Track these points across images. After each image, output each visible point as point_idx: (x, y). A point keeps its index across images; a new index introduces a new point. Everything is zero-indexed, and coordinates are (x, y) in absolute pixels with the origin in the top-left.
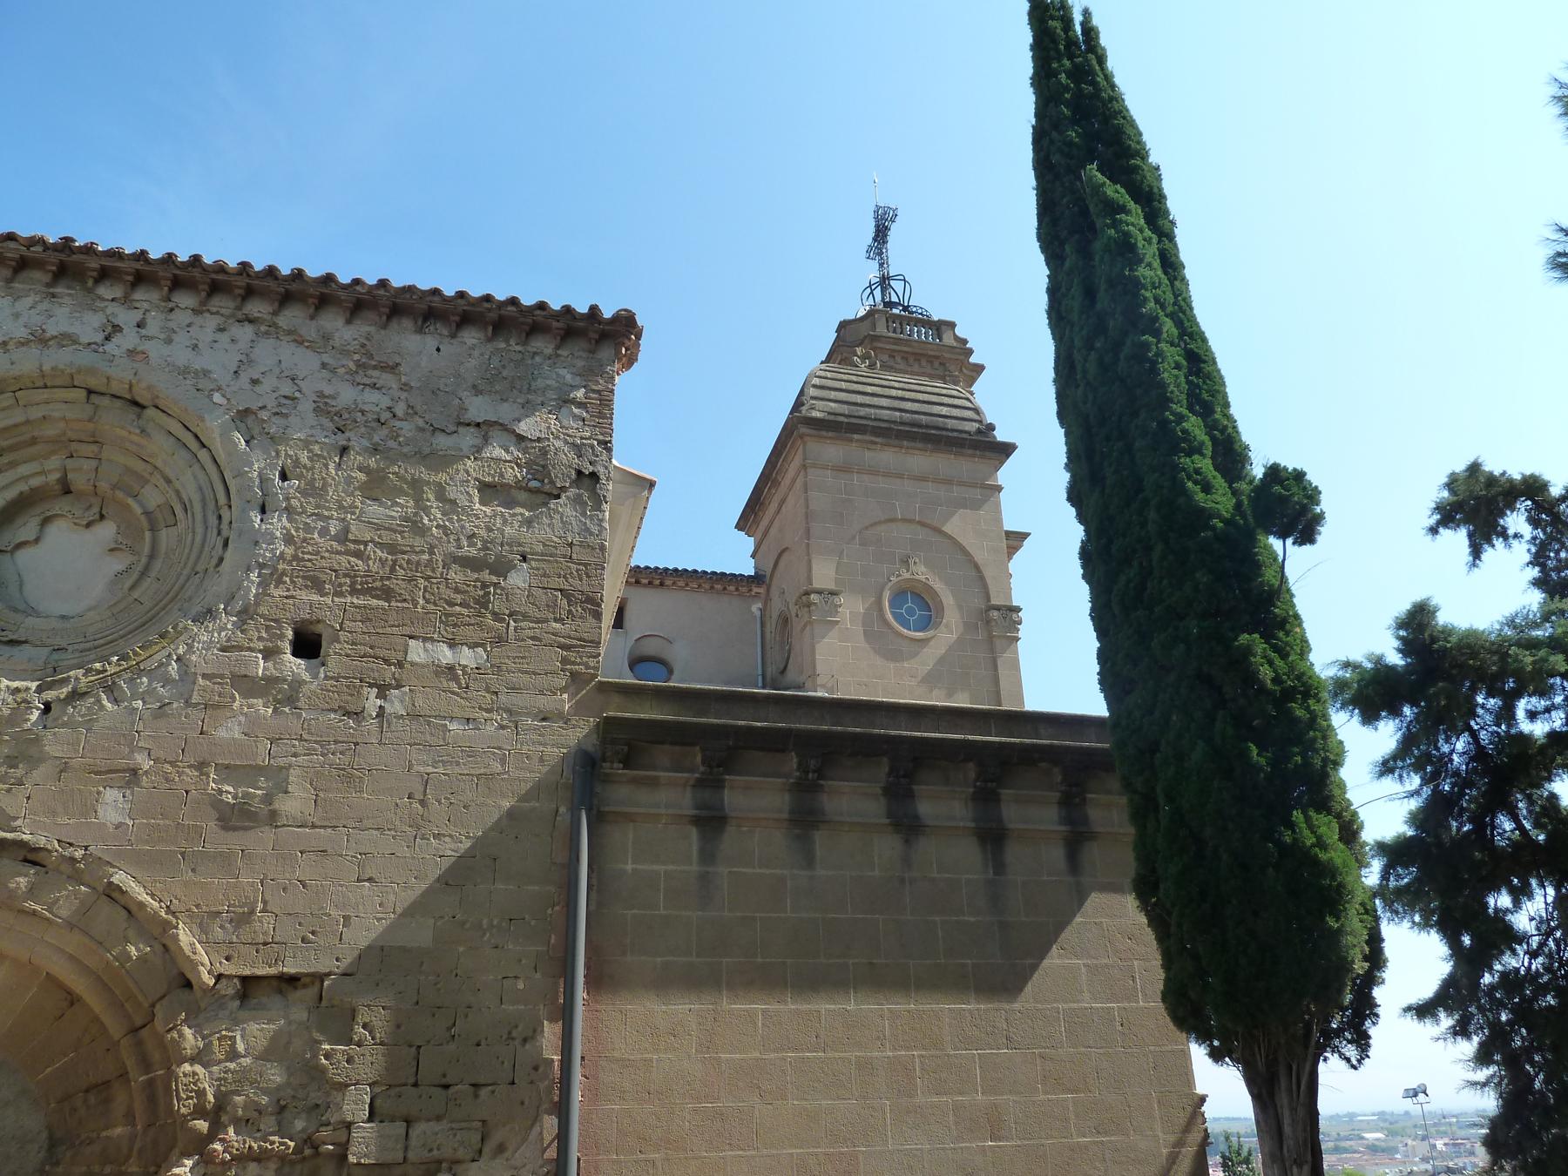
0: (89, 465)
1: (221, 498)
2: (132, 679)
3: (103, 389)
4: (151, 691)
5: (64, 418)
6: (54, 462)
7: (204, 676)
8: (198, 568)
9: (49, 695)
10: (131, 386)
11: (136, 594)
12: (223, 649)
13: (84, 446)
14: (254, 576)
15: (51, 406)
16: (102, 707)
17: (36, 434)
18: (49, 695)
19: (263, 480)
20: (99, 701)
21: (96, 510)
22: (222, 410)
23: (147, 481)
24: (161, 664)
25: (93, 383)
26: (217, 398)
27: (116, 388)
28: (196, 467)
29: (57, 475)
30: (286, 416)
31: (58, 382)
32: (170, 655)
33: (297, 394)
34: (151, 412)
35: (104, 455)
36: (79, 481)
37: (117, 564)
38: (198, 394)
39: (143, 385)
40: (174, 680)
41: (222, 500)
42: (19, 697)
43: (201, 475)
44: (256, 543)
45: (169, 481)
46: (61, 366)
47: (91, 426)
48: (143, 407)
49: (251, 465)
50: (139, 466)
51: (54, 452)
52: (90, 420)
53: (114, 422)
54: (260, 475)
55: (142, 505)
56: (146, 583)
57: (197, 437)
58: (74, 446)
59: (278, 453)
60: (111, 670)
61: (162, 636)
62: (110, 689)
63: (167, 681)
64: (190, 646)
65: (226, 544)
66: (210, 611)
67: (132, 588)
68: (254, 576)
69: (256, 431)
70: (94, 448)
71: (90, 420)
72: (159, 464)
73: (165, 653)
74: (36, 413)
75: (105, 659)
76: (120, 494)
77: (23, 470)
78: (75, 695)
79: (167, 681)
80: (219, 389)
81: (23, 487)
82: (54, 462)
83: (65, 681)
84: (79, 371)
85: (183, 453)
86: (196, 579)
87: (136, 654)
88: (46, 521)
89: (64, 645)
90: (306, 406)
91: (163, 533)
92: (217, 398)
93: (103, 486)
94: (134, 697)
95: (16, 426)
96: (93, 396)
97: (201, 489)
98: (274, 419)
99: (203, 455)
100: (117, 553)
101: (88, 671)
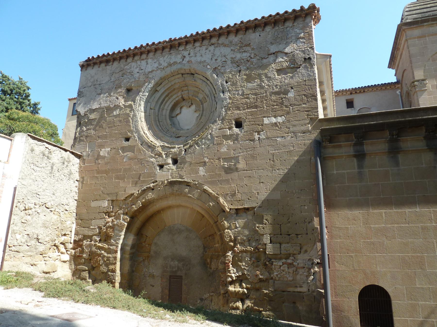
2: (201, 141)
3: (185, 73)
4: (205, 143)
6: (179, 94)
7: (216, 137)
9: (185, 147)
11: (201, 121)
12: (219, 129)
16: (196, 148)
18: (185, 147)
20: (195, 147)
21: (190, 103)
23: (199, 93)
24: (207, 136)
25: (182, 72)
26: (208, 67)
27: (188, 71)
28: (208, 86)
29: (181, 96)
31: (175, 74)
34: (196, 75)
35: (189, 89)
36: (185, 97)
37: (197, 115)
41: (214, 92)
43: (209, 88)
44: (223, 101)
47: (184, 82)
50: (196, 89)
51: (179, 91)
53: (189, 80)
62: (197, 144)
64: (212, 130)
67: (200, 119)
70: (187, 87)
73: (207, 133)
74: (173, 83)
77: (174, 97)
78: (191, 146)
80: (208, 64)
82: (179, 94)
83: (188, 144)
88: (181, 108)
90: (229, 62)
99: (208, 82)
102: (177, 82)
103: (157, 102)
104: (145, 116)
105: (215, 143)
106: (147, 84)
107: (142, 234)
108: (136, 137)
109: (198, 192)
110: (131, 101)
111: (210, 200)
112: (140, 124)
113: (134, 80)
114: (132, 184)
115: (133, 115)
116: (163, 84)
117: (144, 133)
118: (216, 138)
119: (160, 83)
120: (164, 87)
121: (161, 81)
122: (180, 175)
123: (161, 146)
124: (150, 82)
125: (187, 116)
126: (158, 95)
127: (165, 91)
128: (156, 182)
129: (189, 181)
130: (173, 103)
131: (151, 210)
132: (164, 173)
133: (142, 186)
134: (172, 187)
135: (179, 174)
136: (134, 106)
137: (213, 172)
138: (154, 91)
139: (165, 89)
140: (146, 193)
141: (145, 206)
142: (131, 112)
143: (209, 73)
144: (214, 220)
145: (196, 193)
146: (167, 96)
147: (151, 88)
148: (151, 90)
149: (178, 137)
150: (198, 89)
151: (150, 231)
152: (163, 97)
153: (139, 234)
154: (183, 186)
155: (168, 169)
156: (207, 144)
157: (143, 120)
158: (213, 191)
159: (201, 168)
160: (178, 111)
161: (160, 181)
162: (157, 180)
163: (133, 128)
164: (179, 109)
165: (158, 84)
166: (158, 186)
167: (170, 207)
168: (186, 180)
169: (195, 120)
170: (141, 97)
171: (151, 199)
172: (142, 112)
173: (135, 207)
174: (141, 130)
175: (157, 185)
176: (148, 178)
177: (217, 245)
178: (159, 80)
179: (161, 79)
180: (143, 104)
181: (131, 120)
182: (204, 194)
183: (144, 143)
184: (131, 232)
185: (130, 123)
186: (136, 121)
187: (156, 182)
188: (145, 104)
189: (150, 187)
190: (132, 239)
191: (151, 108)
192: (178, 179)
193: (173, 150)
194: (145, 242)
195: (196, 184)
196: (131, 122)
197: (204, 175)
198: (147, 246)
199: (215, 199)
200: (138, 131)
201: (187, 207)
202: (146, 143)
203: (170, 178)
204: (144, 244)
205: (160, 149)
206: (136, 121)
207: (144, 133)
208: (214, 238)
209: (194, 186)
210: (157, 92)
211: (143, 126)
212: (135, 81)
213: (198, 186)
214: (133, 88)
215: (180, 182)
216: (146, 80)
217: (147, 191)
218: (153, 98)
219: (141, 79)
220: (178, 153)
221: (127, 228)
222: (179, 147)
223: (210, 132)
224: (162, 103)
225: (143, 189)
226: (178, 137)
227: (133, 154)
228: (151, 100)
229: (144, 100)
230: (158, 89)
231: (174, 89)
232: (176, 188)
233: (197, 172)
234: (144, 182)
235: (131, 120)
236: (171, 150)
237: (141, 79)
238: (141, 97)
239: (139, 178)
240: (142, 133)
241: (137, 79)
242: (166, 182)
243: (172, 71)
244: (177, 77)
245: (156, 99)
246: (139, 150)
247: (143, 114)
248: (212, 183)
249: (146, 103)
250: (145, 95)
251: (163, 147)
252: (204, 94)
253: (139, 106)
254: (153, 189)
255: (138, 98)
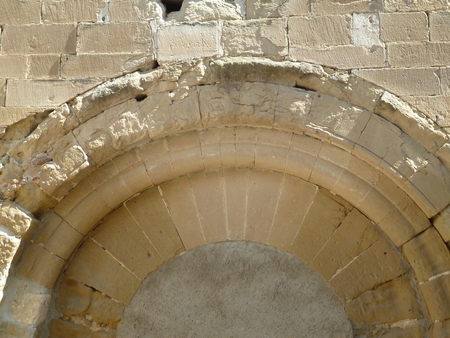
107: (71, 283)
109: (350, 113)
111: (407, 148)
114: (35, 71)
122: (267, 43)
128: (156, 65)
129: (311, 69)
131: (123, 183)
132: (187, 29)
133: (89, 81)
134: (234, 93)
135: (258, 37)
137: (412, 37)
140: (109, 113)
141: (100, 167)
144: (410, 226)
145: (343, 122)
151: (107, 270)
153: (63, 283)
154: (283, 90)
155: (209, 18)
158: (419, 112)
159: (359, 20)
161: (173, 63)
162: (160, 59)
166: (164, 86)
167: (197, 174)
168: (297, 65)
171: (133, 136)
173: (57, 173)
175: (160, 79)
176: (113, 46)
177: (407, 323)
182: (379, 127)
184: (28, 276)
187: (156, 65)
189: (128, 88)
190: (37, 305)
192: (257, 60)
194: (84, 315)
195: (341, 82)
197: (373, 49)
198: (95, 328)
199: (430, 146)
201: (277, 174)
203: (220, 51)
204: (77, 321)
208: (391, 297)
209: (335, 90)
213: (344, 92)
215: (270, 74)
217: (114, 101)
221: (18, 260)
225: (94, 93)
232: (250, 93)
233: (343, 36)
234: (95, 63)
239: (70, 48)
242: (202, 67)
248: (410, 81)
254: (141, 98)
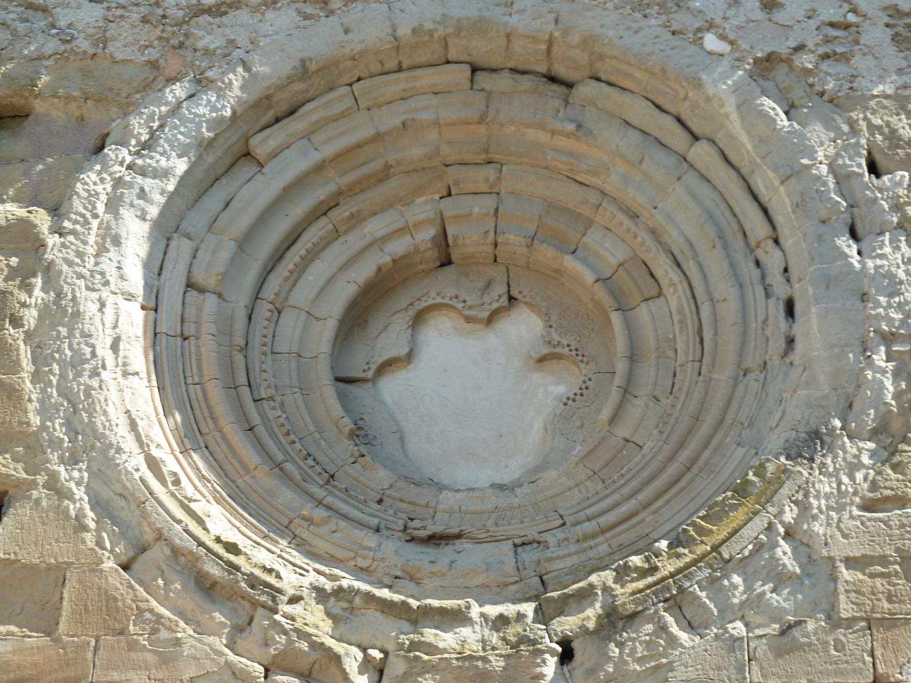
0: (481, 206)
1: (751, 225)
2: (713, 581)
3: (497, 61)
4: (755, 602)
5: (436, 123)
6: (423, 209)
7: (850, 562)
8: (748, 363)
9: (566, 624)
10: (550, 43)
11: (623, 430)
12: (869, 506)
13: (471, 171)
14: (880, 358)
15: (413, 103)
16: (673, 641)
17: (391, 158)
18: (566, 624)
19: (843, 178)
20: (663, 628)
21: (500, 289)
22: (725, 63)
23: (589, 223)
24: (759, 547)
25: (482, 49)
26: (711, 42)
27: (524, 53)
28: (691, 179)
29: (429, 233)
30: (845, 58)
31: (422, 56)
32: (770, 527)
33: (851, 18)
34: (588, 90)
35: (505, 186)
36: (469, 238)
37: (553, 388)
38: (676, 41)
39: (575, 39)
40: (792, 577)
41: (757, 227)
42: (512, 632)
43: (704, 191)
44: (864, 297)
45: (634, 216)
46: (429, 25)
47: (482, 130)
48: (570, 85)
49: (812, 155)
50: (572, 197)
51: (417, 192)
52: (481, 121)
53: (525, 117)
54: (832, 168)
55: (592, 268)
56: (636, 409)
57: (680, 121)
58: (453, 173)
59: (852, 124)
60: (667, 567)
61: (742, 490)
62: (678, 602)
63: (780, 579)
64: (804, 508)
65: (790, 309)
66: (815, 435)
67: (614, 419)
68: (880, 358)
69: (797, 93)
70: (490, 172)
71: (481, 121)
72: (612, 183)
73: (760, 523)
74: (389, 119)
75: (646, 547)
76: (546, 253)
77: (375, 227)
78: (615, 621)
79: (780, 579)
80: (710, 26)
81: (382, 258)
82: (423, 209)
83: (586, 595)
84: (458, 31)
85: (660, 154)
86: (753, 382)
87: (701, 531)
88: (419, 319)
89: (532, 534)
90: (876, 35)
91: (643, 313)
92: (711, 42)
93: (513, 239)
94: (727, 613)
95: (359, 146)
96: (479, 75)
97: (711, 216)
98: (824, 66)
99: (701, 153)
100: (554, 365)
101: (622, 574)
102: (426, 116)
103: (244, 244)
104: (154, 335)
105: (846, 609)
106: (179, 90)
108: (79, 493)
110: (31, 200)
112: (113, 395)
113: (52, 46)
115: (44, 312)
116: (310, 114)
117: (153, 464)
118: (845, 574)
119: (283, 100)
120: (308, 135)
121: (298, 87)
123: (321, 594)
124: (202, 83)
125: (473, 393)
126: (256, 191)
127: (319, 168)
130: (364, 272)
136: (53, 240)
138: (230, 155)
139: (315, 157)
142: (28, 288)
143: (724, 84)
146: (324, 210)
147: (214, 124)
148: (211, 143)
149: (435, 539)
150: (594, 197)
152: (298, 210)
156: (775, 615)
157: (137, 355)
160: (389, 338)
163: (46, 410)
164: (401, 322)
165: (273, 109)
169: (537, 427)
170: (118, 183)
172: (130, 297)
174: (129, 444)
178: (291, 80)
179: (303, 72)
180: (136, 236)
181: (25, 353)
183: (159, 552)
185: (15, 367)
186: (78, 361)
188: (153, 238)
191: (199, 277)
193: (446, 640)
196: (27, 364)
200: (89, 445)
202: (176, 552)
205: (315, 620)
206: (78, 361)
207: (153, 464)
210: (246, 170)
211: (131, 402)
212: (61, 57)
214: (39, 106)
216: (172, 65)
218: (213, 202)
219: (116, 50)
220: (498, 664)
222: (502, 621)
223: (789, 516)
224: (278, 257)
226: (435, 539)
227: (36, 640)
228: (197, 220)
229: (153, 212)
230: (261, 145)
231: (385, 174)
235: (25, 353)
236: (430, 634)
237: (116, 50)
238: (118, 183)
240: (133, 462)
241: (84, 45)
243: (404, 31)
244: (426, 78)
245: (244, 222)
246: (110, 615)
247: (133, 319)
249: (166, 231)
250: (165, 174)
251: (338, 607)
252: (644, 236)
253: (102, 250)
255: (93, 183)
